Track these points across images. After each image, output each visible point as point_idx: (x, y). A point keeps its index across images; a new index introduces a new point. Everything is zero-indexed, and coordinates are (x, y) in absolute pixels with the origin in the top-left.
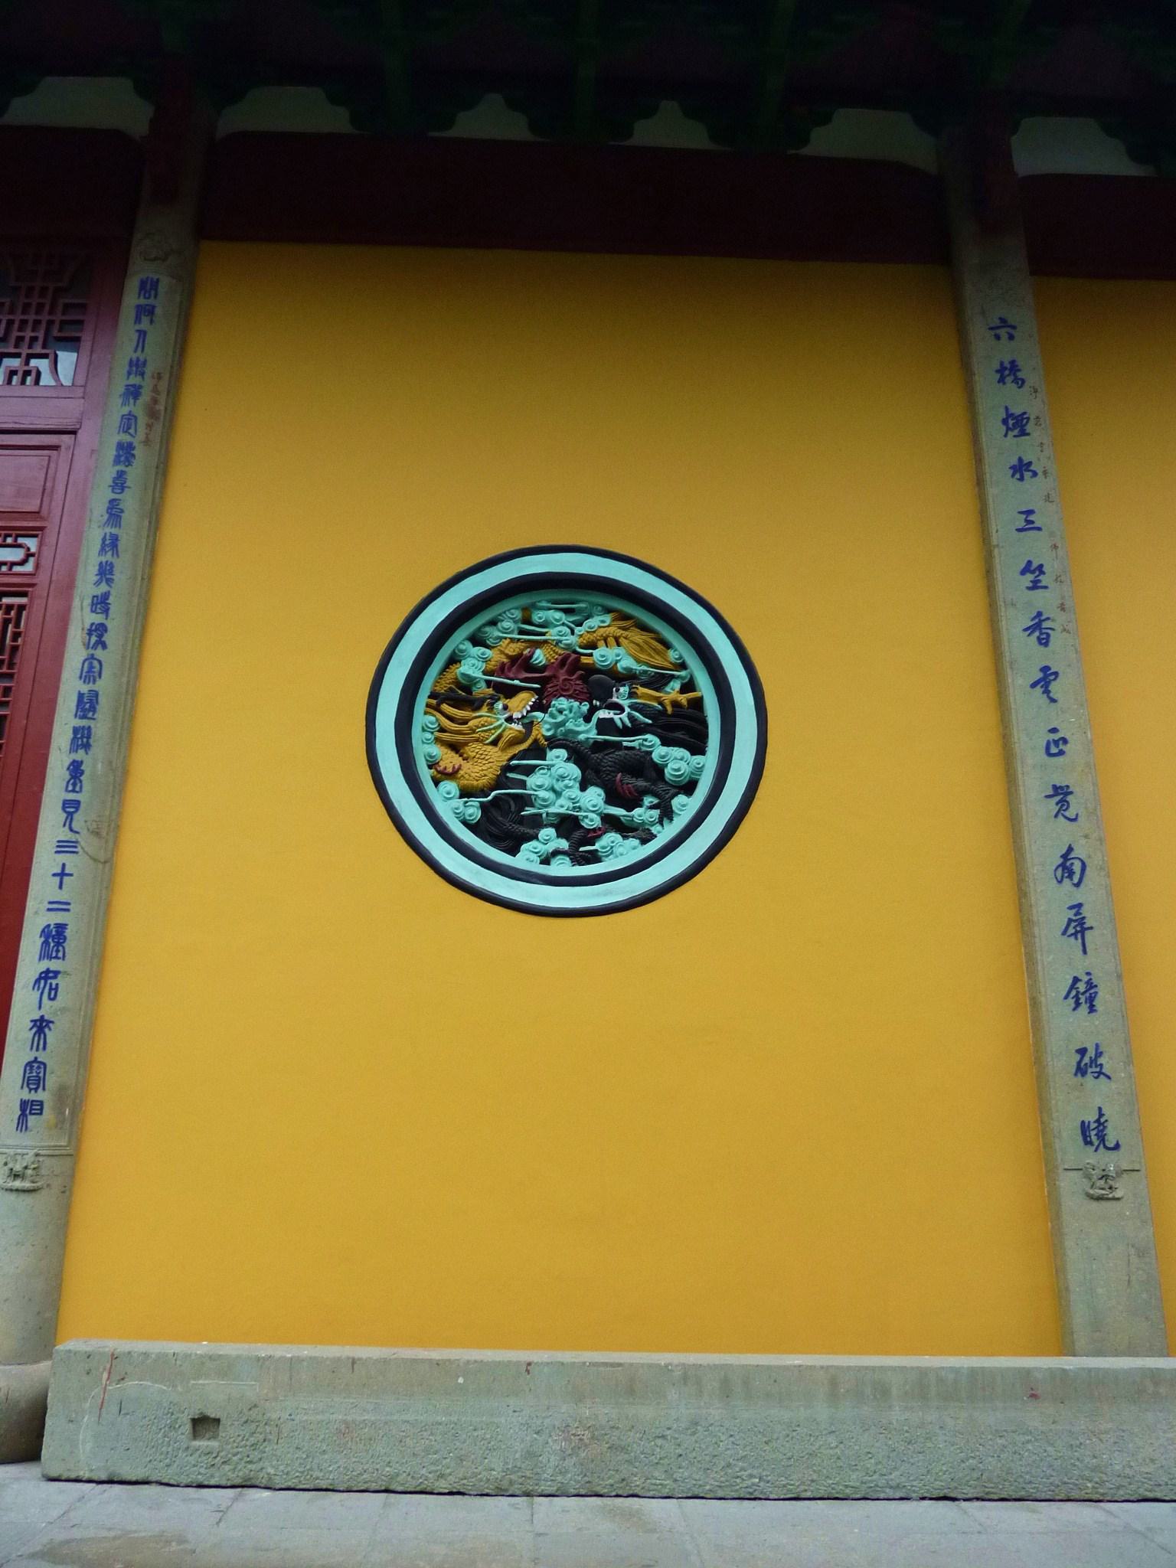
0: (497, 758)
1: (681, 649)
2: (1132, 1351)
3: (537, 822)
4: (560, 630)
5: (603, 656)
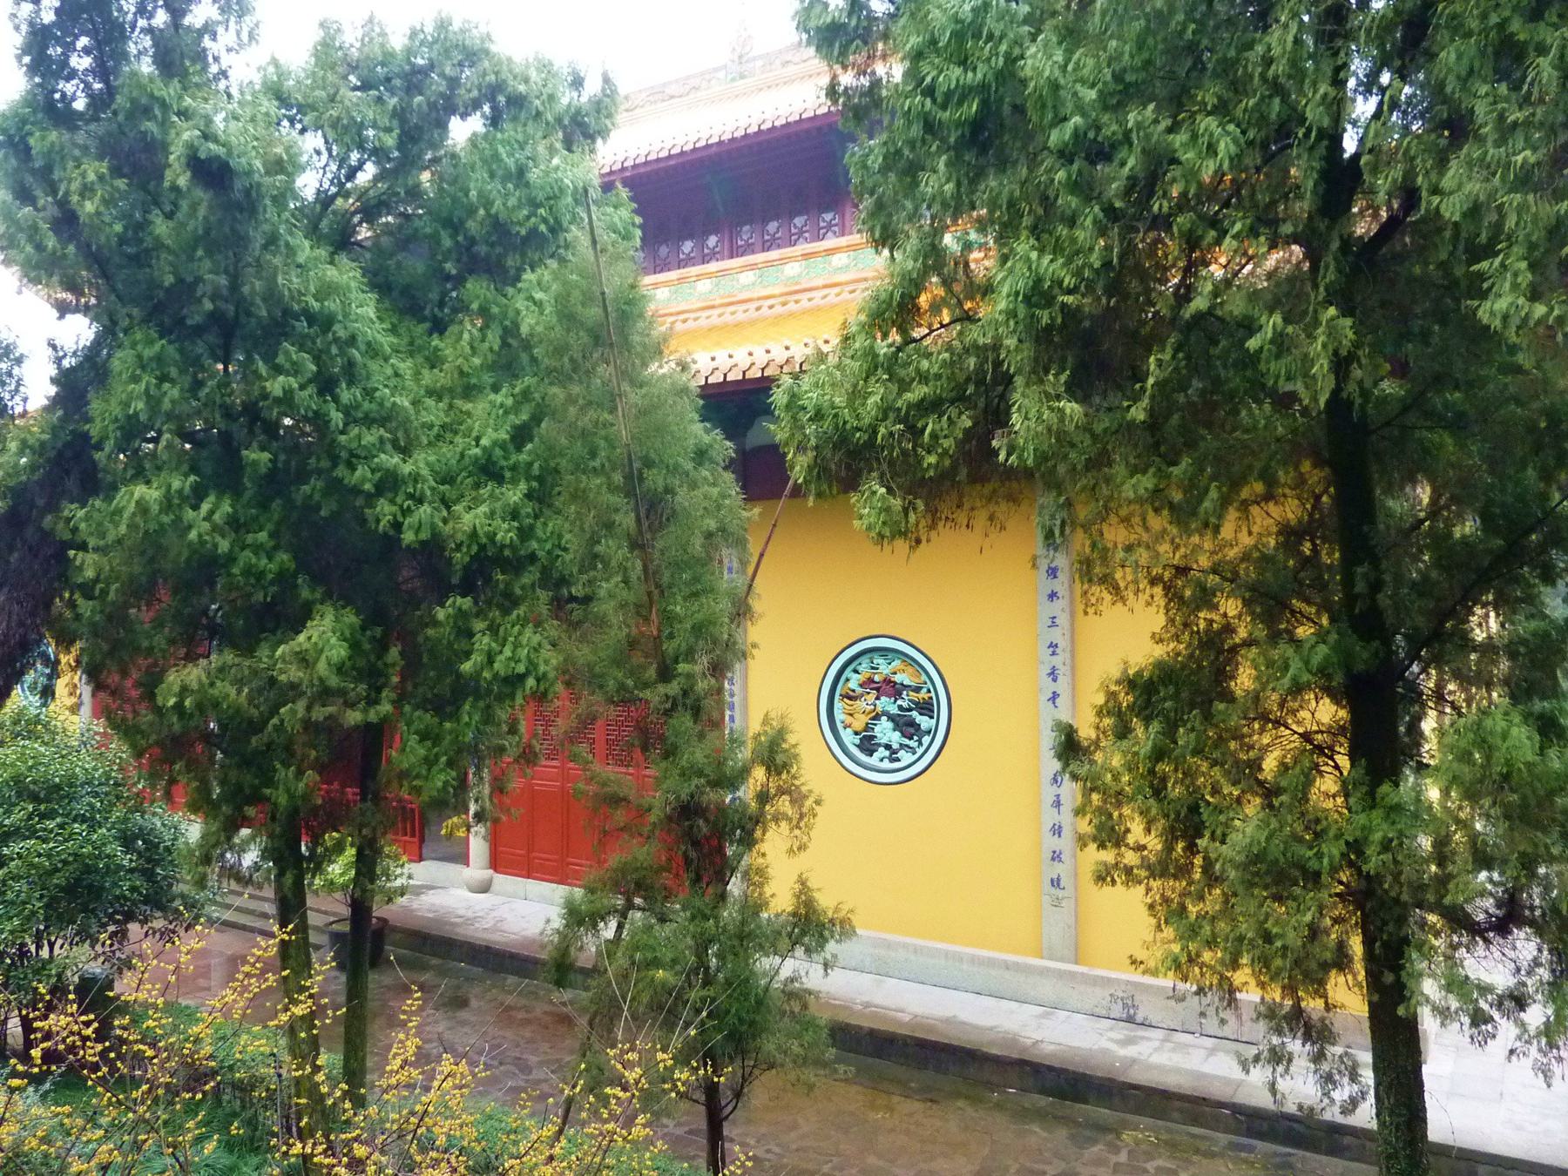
0: (864, 719)
1: (924, 677)
2: (1062, 960)
3: (879, 745)
4: (885, 668)
5: (898, 678)
